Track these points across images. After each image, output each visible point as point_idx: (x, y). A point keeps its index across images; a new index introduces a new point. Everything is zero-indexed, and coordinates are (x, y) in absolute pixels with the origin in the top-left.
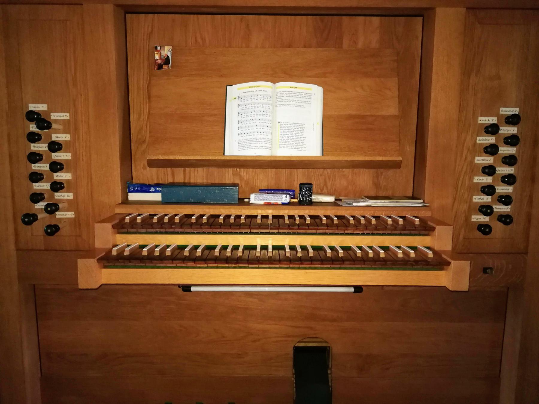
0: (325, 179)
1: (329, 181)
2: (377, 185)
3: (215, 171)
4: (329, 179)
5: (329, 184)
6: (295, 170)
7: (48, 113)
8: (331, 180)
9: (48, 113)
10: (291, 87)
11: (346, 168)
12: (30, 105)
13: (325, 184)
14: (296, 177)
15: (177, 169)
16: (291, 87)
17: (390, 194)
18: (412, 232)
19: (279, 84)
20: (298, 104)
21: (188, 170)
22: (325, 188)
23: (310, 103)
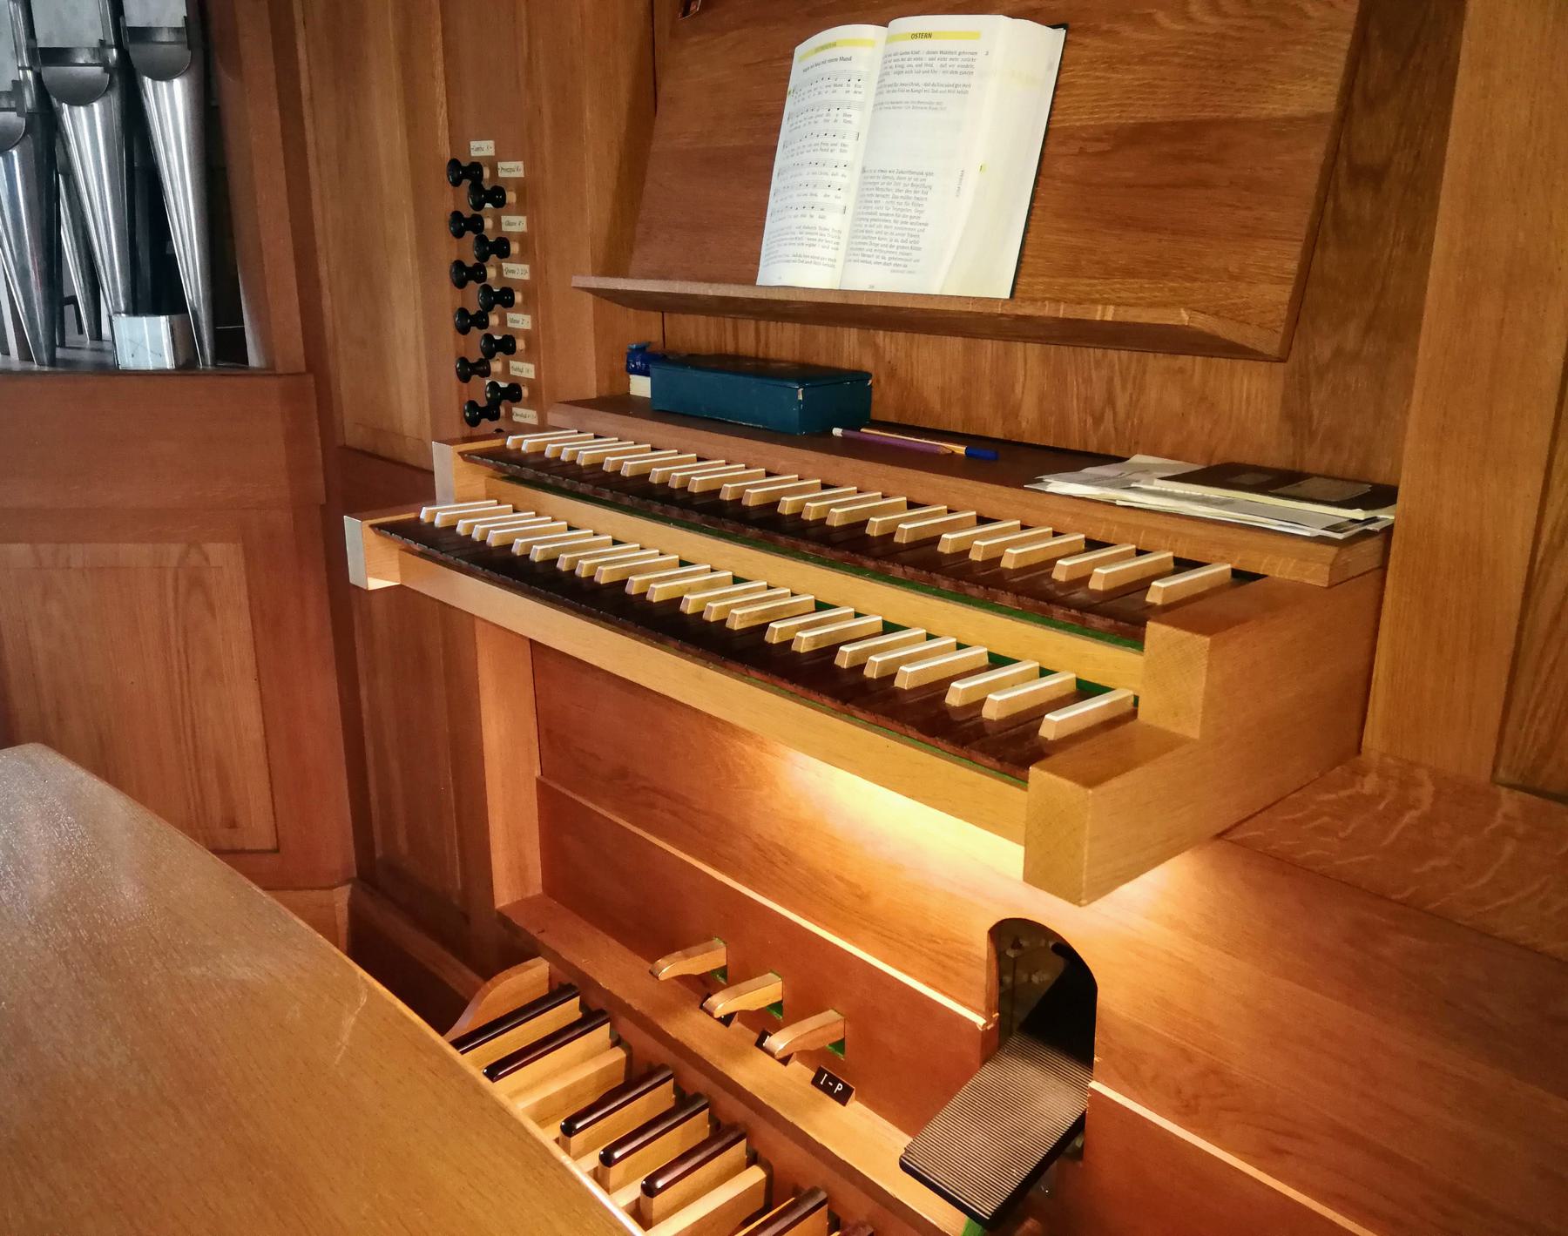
0: (1110, 380)
1: (1124, 388)
2: (1296, 419)
3: (822, 333)
4: (1124, 381)
5: (1122, 401)
6: (1020, 345)
7: (493, 164)
8: (1129, 386)
9: (493, 164)
10: (915, 36)
11: (1261, 354)
12: (474, 144)
13: (1111, 401)
14: (1020, 363)
15: (846, 330)
16: (915, 36)
17: (1353, 465)
18: (565, 484)
19: (895, 23)
20: (923, 97)
21: (762, 324)
22: (1109, 415)
23: (962, 90)
